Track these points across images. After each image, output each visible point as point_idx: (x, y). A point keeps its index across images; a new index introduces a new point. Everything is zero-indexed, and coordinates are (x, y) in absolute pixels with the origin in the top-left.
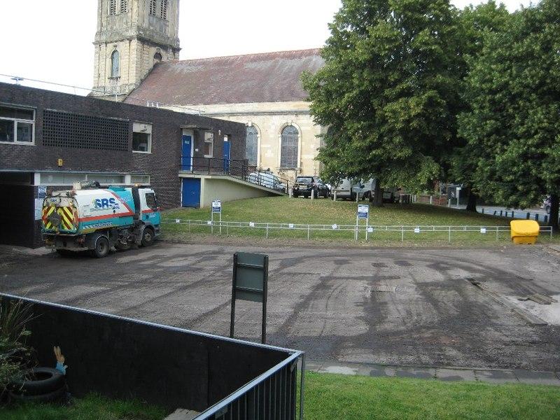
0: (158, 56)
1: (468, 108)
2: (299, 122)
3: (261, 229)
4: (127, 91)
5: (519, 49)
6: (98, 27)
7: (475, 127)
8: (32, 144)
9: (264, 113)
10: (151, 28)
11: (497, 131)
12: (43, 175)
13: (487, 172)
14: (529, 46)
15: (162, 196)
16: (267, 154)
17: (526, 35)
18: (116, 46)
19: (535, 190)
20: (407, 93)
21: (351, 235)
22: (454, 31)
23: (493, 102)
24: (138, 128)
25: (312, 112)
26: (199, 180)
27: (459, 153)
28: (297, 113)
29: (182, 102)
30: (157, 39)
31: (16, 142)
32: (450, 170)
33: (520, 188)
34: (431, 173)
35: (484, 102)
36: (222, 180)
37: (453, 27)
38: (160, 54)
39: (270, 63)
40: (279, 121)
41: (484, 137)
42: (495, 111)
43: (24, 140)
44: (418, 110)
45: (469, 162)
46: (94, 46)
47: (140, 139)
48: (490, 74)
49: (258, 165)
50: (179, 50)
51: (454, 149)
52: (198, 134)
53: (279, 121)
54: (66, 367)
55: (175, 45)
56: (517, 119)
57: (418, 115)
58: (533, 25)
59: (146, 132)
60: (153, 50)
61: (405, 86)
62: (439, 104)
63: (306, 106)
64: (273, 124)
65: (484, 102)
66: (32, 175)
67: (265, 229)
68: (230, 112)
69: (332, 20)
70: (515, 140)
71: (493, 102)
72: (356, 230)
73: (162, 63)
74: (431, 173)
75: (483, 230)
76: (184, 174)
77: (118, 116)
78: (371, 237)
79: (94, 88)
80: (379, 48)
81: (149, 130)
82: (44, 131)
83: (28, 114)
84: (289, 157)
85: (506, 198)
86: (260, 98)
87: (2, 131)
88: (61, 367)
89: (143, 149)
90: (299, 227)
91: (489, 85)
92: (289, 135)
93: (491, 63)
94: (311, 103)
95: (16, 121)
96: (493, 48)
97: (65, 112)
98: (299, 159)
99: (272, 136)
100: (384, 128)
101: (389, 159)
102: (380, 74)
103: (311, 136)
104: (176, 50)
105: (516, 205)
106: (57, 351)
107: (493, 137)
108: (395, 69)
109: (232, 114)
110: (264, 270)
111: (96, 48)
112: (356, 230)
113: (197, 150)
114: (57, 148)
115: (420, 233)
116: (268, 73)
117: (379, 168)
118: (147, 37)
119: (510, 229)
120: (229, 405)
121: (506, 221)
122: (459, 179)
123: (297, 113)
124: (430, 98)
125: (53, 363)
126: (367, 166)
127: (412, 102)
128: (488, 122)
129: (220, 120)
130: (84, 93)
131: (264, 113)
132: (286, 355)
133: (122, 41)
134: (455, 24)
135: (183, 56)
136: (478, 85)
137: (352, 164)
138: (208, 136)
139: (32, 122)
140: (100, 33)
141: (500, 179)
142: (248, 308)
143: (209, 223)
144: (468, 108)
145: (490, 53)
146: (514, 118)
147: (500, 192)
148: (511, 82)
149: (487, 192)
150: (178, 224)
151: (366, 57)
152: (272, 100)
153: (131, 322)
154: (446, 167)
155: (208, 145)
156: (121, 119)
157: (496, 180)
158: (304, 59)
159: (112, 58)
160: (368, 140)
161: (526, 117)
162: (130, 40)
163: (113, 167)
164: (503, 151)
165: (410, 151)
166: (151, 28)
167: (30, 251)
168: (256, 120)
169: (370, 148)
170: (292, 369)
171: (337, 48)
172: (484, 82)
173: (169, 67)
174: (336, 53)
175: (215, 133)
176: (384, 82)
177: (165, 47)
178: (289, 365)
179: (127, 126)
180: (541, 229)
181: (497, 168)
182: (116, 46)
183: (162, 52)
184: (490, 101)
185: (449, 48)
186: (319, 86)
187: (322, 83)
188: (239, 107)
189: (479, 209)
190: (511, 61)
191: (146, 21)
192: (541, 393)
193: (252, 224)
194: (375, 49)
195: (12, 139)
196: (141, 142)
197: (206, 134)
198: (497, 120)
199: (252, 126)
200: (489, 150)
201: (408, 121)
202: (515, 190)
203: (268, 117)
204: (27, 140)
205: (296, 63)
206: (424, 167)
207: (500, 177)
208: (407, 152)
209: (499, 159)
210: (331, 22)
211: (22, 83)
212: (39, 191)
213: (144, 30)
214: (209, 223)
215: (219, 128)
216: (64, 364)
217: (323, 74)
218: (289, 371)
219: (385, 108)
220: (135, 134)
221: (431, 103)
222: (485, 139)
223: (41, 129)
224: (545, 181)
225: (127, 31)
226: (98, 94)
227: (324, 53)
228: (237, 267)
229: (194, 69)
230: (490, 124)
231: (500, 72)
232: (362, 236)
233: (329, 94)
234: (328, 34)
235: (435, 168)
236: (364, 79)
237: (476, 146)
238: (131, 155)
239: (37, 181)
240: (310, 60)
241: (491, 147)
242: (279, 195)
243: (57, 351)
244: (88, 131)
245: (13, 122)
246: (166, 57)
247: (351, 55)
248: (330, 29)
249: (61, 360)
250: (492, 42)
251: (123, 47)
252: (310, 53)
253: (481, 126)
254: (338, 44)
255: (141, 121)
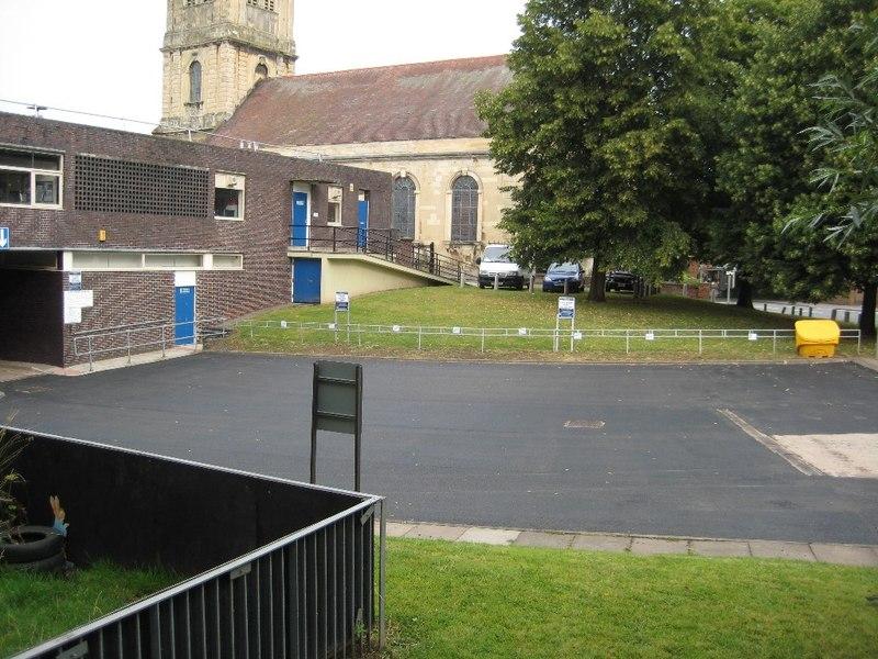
0: (262, 68)
1: (732, 146)
2: (479, 170)
3: (411, 335)
4: (214, 124)
5: (812, 50)
6: (168, 24)
7: (741, 174)
8: (59, 207)
9: (423, 157)
10: (251, 25)
11: (776, 181)
12: (77, 255)
13: (759, 244)
14: (826, 48)
15: (263, 287)
16: (432, 221)
17: (822, 30)
18: (195, 54)
19: (834, 272)
20: (639, 123)
21: (548, 345)
22: (712, 24)
23: (769, 137)
24: (221, 181)
25: (493, 154)
26: (319, 261)
27: (721, 217)
28: (476, 156)
29: (296, 141)
30: (259, 42)
31: (34, 205)
32: (706, 244)
33: (810, 269)
34: (677, 247)
35: (754, 135)
36: (343, 260)
37: (712, 18)
38: (264, 66)
39: (435, 78)
40: (448, 169)
41: (756, 190)
42: (771, 150)
43: (45, 203)
44: (656, 150)
45: (736, 230)
46: (162, 54)
47: (226, 199)
48: (765, 91)
49: (417, 238)
50: (294, 58)
51: (714, 210)
52: (317, 189)
53: (448, 169)
54: (66, 525)
55: (288, 52)
56: (807, 162)
57: (656, 157)
58: (834, 14)
59: (235, 188)
60: (254, 60)
61: (635, 111)
62: (687, 140)
63: (484, 144)
64: (439, 173)
65: (754, 135)
66: (60, 254)
67: (417, 336)
68: (372, 155)
69: (522, 10)
70: (803, 195)
71: (769, 137)
72: (556, 337)
73: (268, 80)
74: (677, 247)
75: (753, 337)
76: (296, 251)
77: (192, 164)
78: (581, 348)
79: (163, 120)
80: (594, 53)
81: (240, 183)
82: (76, 188)
83: (50, 160)
84: (464, 227)
85: (791, 286)
86: (416, 135)
87: (12, 187)
88: (61, 525)
89: (231, 214)
90: (472, 332)
91: (762, 109)
92: (464, 190)
93: (769, 75)
94: (490, 140)
95: (34, 172)
96: (772, 52)
97: (108, 157)
98: (479, 227)
99: (437, 192)
100: (603, 180)
101: (612, 225)
102: (596, 94)
103: (497, 191)
104: (290, 59)
105: (805, 297)
106: (55, 502)
107: (769, 190)
108: (619, 87)
109: (376, 159)
110: (356, 386)
111: (165, 57)
112: (556, 337)
113: (316, 215)
114: (95, 213)
115: (655, 341)
116: (434, 94)
117: (596, 240)
118: (245, 40)
119: (794, 333)
120: (253, 563)
121: (788, 322)
122: (720, 257)
123: (476, 156)
124: (675, 131)
125: (49, 520)
126: (578, 237)
127: (647, 137)
128: (761, 167)
129: (351, 168)
130: (148, 131)
131: (423, 157)
132: (358, 500)
133: (206, 45)
134: (715, 13)
135: (301, 68)
136: (745, 110)
137: (553, 234)
138: (334, 194)
139: (60, 173)
140: (170, 35)
141: (782, 257)
142: (335, 442)
143: (332, 326)
144: (732, 146)
145: (766, 60)
146: (803, 160)
147: (780, 277)
148: (795, 106)
149: (761, 276)
150: (284, 330)
151: (573, 66)
152: (434, 137)
153: (153, 459)
154: (700, 239)
155: (332, 207)
156: (196, 168)
157: (775, 258)
158: (488, 71)
159: (191, 73)
160: (578, 198)
161: (822, 160)
162: (218, 44)
163: (186, 242)
164: (785, 213)
165: (102, 232)
166: (251, 25)
167: (56, 371)
168: (413, 168)
169: (581, 211)
170: (363, 520)
171: (532, 53)
172: (757, 104)
173: (278, 85)
174: (528, 60)
175: (345, 189)
176: (605, 108)
177: (273, 55)
178: (358, 514)
179: (206, 178)
180: (842, 334)
181: (775, 239)
182: (195, 54)
183: (268, 62)
184: (763, 133)
185: (706, 53)
186: (503, 114)
187: (509, 109)
188: (387, 148)
189: (758, 306)
190: (799, 71)
191: (243, 14)
192: (768, 568)
193: (396, 328)
194: (588, 55)
195: (28, 201)
196: (231, 202)
197: (330, 189)
198: (775, 164)
199: (407, 177)
200: (762, 210)
201: (641, 167)
202: (803, 274)
203: (432, 162)
204: (52, 202)
205: (478, 78)
206: (667, 239)
207: (781, 253)
208: (639, 215)
209: (777, 224)
210: (522, 12)
211: (46, 115)
212: (72, 279)
213: (238, 29)
214: (332, 326)
215: (352, 181)
216: (65, 522)
217: (507, 95)
218: (360, 528)
219: (604, 148)
220: (218, 191)
221: (676, 138)
222: (757, 194)
223: (72, 184)
224: (847, 259)
225: (213, 29)
226: (170, 128)
227: (514, 61)
228: (318, 383)
229: (317, 89)
230: (765, 171)
231: (779, 89)
232: (564, 346)
233: (518, 125)
234: (518, 33)
235: (684, 240)
236: (572, 103)
237: (743, 205)
238: (213, 223)
239: (68, 264)
240: (496, 74)
241: (765, 205)
242: (446, 284)
243: (55, 502)
244: (142, 183)
245: (28, 174)
246: (276, 69)
247: (544, 64)
248: (519, 24)
249: (60, 515)
250: (771, 41)
251: (206, 56)
252: (494, 61)
253: (751, 174)
254: (532, 47)
255: (228, 170)
